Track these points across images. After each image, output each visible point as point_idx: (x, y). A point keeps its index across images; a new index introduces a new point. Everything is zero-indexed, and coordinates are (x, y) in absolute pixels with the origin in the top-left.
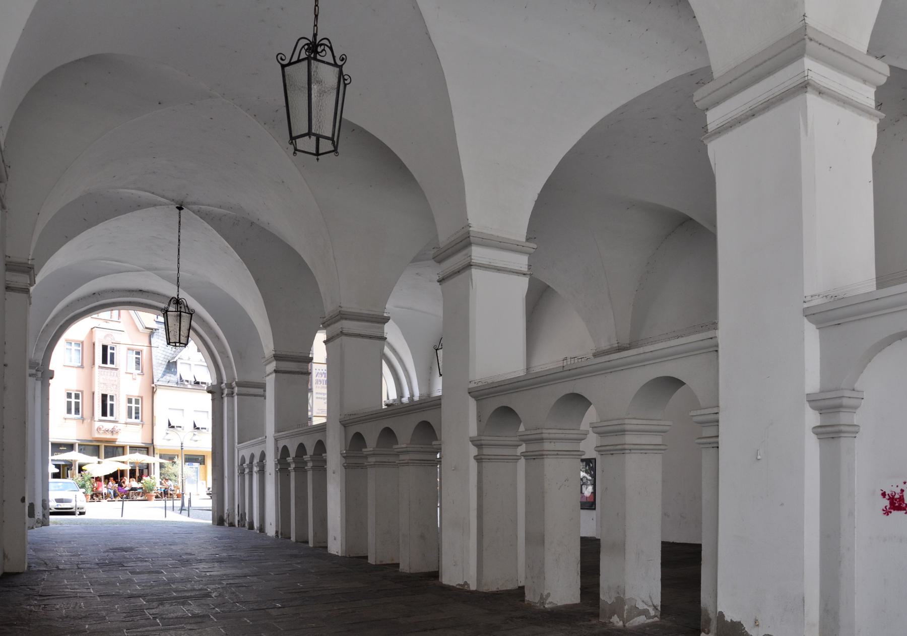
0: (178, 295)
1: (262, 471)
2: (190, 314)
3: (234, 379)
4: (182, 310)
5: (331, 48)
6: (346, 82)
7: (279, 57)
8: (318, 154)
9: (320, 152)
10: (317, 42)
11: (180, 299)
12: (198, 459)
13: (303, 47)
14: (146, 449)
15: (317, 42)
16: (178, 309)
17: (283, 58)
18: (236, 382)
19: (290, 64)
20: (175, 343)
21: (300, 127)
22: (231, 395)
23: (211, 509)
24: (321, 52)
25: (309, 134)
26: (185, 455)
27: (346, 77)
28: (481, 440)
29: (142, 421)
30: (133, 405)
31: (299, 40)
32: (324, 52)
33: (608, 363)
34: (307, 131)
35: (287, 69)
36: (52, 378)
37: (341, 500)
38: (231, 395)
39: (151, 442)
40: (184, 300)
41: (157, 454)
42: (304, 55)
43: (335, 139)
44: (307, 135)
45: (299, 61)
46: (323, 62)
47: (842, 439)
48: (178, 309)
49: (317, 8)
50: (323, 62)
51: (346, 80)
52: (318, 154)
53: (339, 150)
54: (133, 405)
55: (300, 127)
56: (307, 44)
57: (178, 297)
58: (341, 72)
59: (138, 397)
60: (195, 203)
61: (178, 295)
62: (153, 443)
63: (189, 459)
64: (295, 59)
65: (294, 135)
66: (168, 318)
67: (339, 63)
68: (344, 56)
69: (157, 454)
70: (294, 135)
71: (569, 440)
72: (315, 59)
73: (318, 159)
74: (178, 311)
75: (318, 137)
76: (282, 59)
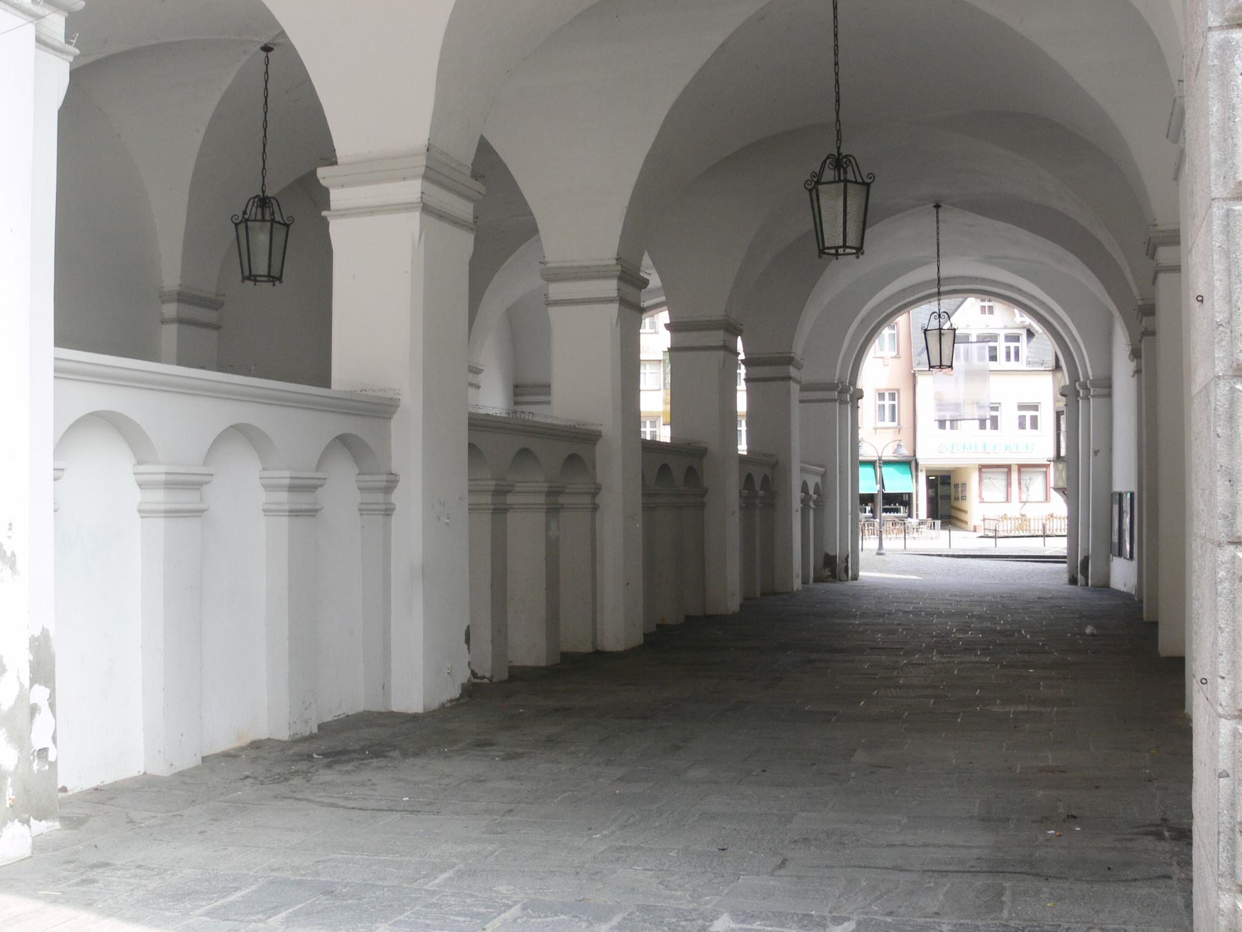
0: (838, 148)
1: (805, 502)
2: (864, 183)
3: (1088, 378)
4: (848, 178)
11: (845, 157)
14: (1006, 470)
16: (839, 177)
18: (1091, 381)
20: (837, 248)
22: (1086, 398)
23: (1065, 534)
29: (899, 424)
30: (887, 402)
36: (861, 397)
37: (1192, 698)
38: (1086, 398)
39: (912, 455)
40: (851, 159)
41: (921, 471)
48: (839, 177)
54: (887, 402)
57: (839, 154)
59: (895, 390)
60: (1150, 333)
61: (838, 148)
62: (915, 455)
66: (821, 198)
69: (921, 471)
74: (839, 181)
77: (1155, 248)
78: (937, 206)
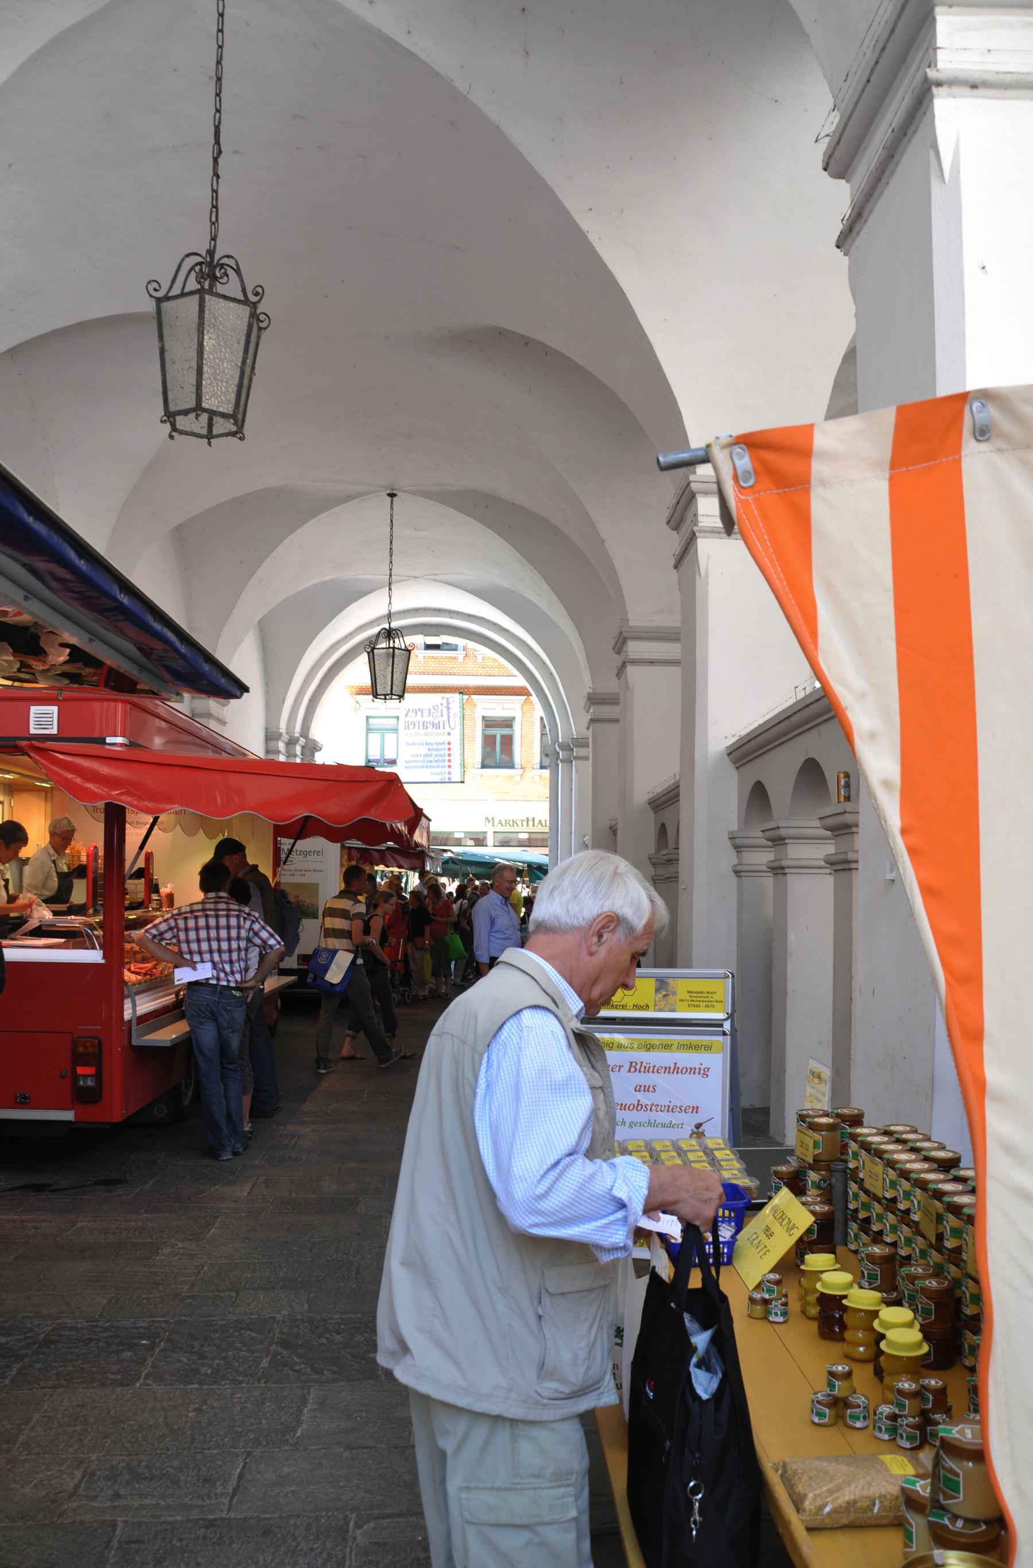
5: (238, 271)
6: (262, 325)
7: (151, 287)
8: (210, 436)
9: (215, 432)
10: (215, 261)
12: (624, 1107)
13: (192, 269)
15: (215, 261)
17: (156, 285)
19: (167, 298)
21: (182, 399)
24: (222, 278)
25: (198, 409)
26: (317, 918)
27: (262, 317)
28: (778, 828)
31: (188, 255)
32: (225, 278)
33: (786, 722)
34: (192, 404)
35: (165, 305)
42: (192, 285)
43: (240, 417)
44: (197, 404)
45: (183, 295)
46: (225, 297)
47: (789, 846)
49: (213, 219)
50: (225, 297)
51: (262, 322)
52: (210, 436)
53: (246, 430)
55: (182, 399)
56: (200, 264)
58: (254, 316)
63: (742, 758)
64: (176, 291)
65: (173, 408)
67: (253, 299)
68: (259, 290)
70: (173, 408)
71: (818, 839)
72: (211, 292)
73: (209, 444)
75: (212, 413)
76: (155, 290)
77: (625, 640)
78: (392, 495)
